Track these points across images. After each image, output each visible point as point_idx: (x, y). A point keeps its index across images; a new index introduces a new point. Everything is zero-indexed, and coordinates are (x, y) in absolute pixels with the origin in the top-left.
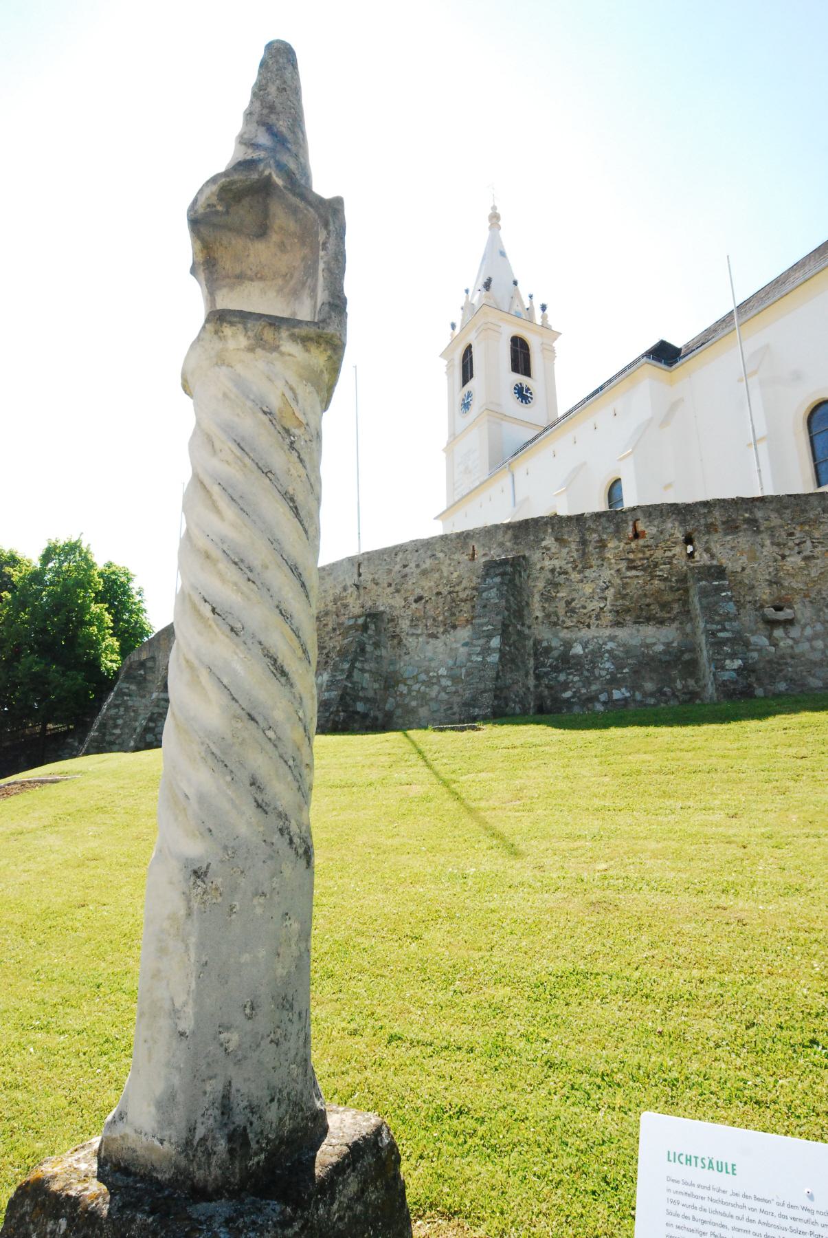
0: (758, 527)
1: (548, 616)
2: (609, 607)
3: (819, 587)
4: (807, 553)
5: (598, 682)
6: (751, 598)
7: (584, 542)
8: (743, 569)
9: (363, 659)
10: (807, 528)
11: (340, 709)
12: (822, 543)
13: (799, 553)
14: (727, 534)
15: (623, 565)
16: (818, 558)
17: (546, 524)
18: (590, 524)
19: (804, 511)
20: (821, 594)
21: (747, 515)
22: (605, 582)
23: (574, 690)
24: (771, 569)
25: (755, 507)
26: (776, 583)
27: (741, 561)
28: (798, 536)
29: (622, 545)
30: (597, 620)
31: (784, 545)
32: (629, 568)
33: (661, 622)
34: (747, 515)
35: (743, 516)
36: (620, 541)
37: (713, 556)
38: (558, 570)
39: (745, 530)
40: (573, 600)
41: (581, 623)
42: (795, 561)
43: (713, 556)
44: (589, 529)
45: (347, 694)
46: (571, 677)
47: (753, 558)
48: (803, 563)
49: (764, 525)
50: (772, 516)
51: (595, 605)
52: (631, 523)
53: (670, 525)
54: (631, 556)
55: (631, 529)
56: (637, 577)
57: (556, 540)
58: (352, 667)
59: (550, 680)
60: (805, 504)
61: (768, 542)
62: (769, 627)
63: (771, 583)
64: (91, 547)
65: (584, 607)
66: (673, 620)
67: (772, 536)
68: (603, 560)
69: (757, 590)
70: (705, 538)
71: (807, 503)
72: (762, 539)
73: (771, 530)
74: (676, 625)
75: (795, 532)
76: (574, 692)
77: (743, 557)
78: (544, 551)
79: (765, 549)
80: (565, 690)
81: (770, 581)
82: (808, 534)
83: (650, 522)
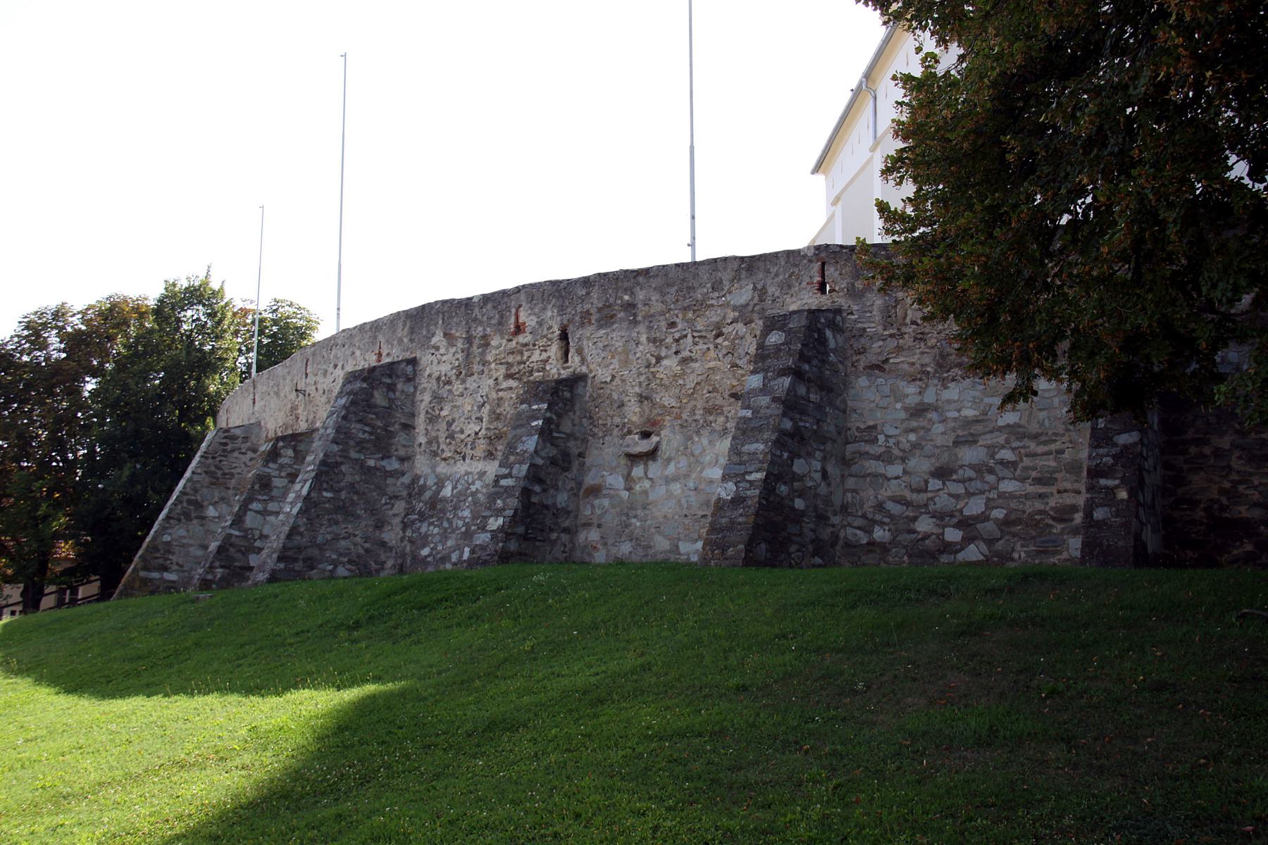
0: (635, 315)
1: (429, 443)
2: (483, 432)
3: (695, 403)
4: (686, 354)
5: (454, 536)
6: (619, 420)
7: (469, 340)
8: (613, 377)
9: (265, 497)
10: (690, 315)
11: (217, 564)
12: (705, 337)
13: (676, 353)
14: (600, 327)
15: (502, 370)
16: (696, 361)
17: (438, 312)
19: (691, 289)
20: (695, 414)
21: (626, 297)
22: (482, 396)
23: (432, 545)
24: (642, 378)
25: (638, 284)
26: (647, 398)
27: (612, 367)
28: (680, 326)
29: (504, 342)
30: (472, 449)
31: (662, 341)
32: (509, 376)
34: (626, 297)
35: (621, 298)
36: (502, 338)
38: (443, 378)
39: (622, 320)
40: (454, 420)
41: (458, 453)
42: (671, 363)
43: (583, 361)
44: (475, 320)
45: (231, 545)
46: (431, 528)
47: (625, 363)
48: (679, 368)
49: (642, 311)
50: (653, 298)
51: (473, 428)
52: (513, 311)
53: (549, 314)
54: (510, 359)
55: (513, 320)
56: (511, 388)
57: (445, 335)
58: (245, 507)
59: (413, 532)
60: (694, 278)
61: (643, 338)
62: (629, 463)
63: (642, 398)
64: (225, 284)
65: (462, 432)
67: (650, 328)
68: (484, 365)
69: (626, 408)
71: (696, 276)
72: (638, 333)
73: (650, 317)
75: (678, 320)
76: (432, 549)
77: (614, 361)
78: (433, 351)
79: (641, 348)
80: (424, 546)
81: (640, 395)
82: (691, 323)
83: (531, 309)
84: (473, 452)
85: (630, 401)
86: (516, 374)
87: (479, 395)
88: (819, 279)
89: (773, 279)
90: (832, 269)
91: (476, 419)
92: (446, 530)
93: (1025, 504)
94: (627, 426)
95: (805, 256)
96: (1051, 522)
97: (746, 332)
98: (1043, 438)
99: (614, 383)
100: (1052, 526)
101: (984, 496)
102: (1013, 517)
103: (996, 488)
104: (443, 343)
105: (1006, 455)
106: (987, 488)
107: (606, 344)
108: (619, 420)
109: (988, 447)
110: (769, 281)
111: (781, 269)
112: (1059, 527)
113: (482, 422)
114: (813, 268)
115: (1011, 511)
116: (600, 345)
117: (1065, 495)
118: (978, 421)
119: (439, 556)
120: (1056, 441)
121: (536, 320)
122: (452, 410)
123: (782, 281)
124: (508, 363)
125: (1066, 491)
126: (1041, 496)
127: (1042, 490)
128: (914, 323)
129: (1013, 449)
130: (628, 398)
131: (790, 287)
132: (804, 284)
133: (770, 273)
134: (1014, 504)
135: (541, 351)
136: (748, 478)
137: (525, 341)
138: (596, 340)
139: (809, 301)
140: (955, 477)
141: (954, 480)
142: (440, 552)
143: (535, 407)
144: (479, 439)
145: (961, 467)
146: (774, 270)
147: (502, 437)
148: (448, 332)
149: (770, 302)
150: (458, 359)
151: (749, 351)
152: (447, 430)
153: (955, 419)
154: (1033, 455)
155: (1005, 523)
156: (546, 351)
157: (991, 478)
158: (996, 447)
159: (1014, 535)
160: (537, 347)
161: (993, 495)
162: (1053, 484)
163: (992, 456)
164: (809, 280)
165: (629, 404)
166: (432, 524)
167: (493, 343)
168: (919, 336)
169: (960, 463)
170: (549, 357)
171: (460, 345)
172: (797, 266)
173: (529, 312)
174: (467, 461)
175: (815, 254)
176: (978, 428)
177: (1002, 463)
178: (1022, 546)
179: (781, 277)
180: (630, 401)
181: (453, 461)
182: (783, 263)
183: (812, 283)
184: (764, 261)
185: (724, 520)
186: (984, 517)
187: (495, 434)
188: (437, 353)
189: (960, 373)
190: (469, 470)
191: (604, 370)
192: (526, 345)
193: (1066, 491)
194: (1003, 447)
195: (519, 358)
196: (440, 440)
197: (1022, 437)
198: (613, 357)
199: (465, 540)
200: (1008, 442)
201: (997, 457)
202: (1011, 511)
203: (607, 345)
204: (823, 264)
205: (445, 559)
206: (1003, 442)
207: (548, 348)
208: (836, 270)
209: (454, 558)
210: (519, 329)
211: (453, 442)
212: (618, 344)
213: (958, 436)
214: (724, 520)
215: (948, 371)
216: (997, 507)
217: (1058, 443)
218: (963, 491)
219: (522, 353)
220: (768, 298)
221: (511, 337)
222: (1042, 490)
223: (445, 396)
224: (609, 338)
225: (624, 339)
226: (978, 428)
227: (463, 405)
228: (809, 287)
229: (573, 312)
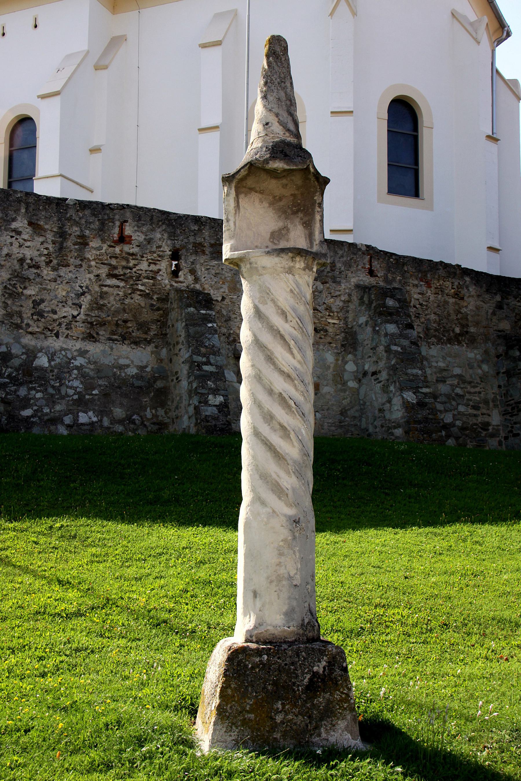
2: (82, 317)
5: (64, 402)
7: (62, 235)
8: (223, 299)
18: (71, 212)
23: (35, 408)
27: (222, 290)
29: (105, 247)
33: (136, 343)
37: (197, 280)
40: (42, 301)
43: (197, 280)
51: (69, 311)
52: (118, 223)
54: (114, 262)
55: (117, 230)
56: (118, 287)
57: (30, 224)
65: (54, 312)
66: (149, 342)
69: (232, 323)
70: (192, 258)
74: (150, 348)
78: (13, 234)
80: (24, 408)
83: (138, 227)
84: (68, 332)
85: (236, 318)
86: (121, 275)
87: (77, 285)
88: (369, 266)
89: (340, 258)
90: (376, 263)
91: (73, 304)
92: (52, 395)
93: (469, 419)
94: (232, 336)
95: (360, 249)
96: (480, 430)
97: (323, 289)
98: (473, 384)
99: (225, 302)
100: (481, 432)
101: (452, 413)
102: (465, 426)
103: (457, 409)
104: (27, 230)
105: (458, 391)
106: (452, 408)
107: (217, 272)
108: (226, 330)
109: (451, 385)
110: (337, 259)
111: (345, 253)
112: (484, 433)
113: (80, 307)
114: (365, 258)
115: (464, 423)
116: (213, 272)
117: (485, 416)
118: (445, 370)
119: (46, 418)
120: (477, 386)
121: (143, 237)
122: (40, 291)
123: (345, 261)
124: (110, 265)
125: (484, 414)
126: (475, 416)
127: (475, 412)
128: (415, 306)
129: (462, 388)
130: (235, 316)
131: (350, 266)
132: (360, 267)
133: (338, 254)
134: (464, 419)
135: (150, 263)
136: (420, 390)
137: (131, 251)
138: (208, 267)
139: (364, 279)
140: (438, 400)
141: (438, 402)
142: (47, 414)
143: (203, 312)
144: (76, 322)
145: (441, 395)
146: (340, 252)
147: (105, 324)
148: (33, 221)
149: (338, 273)
150: (47, 249)
151: (326, 302)
152: (33, 308)
153: (436, 367)
154: (470, 393)
155: (463, 429)
156: (155, 264)
157: (454, 403)
158: (454, 386)
159: (467, 436)
160: (145, 259)
161: (455, 413)
162: (479, 410)
163: (453, 390)
164: (363, 265)
165: (235, 320)
166: (34, 388)
167: (92, 244)
168: (417, 315)
169: (439, 392)
170: (160, 270)
171: (50, 236)
172: (355, 254)
173: (136, 228)
174: (61, 339)
175: (367, 250)
176: (445, 374)
177: (457, 395)
178: (471, 442)
179: (345, 259)
180: (236, 318)
181: (43, 336)
182: (346, 250)
183: (365, 268)
184: (334, 244)
185: (419, 416)
186: (452, 425)
187: (97, 321)
188: (18, 237)
189: (435, 341)
190: (65, 346)
191: (216, 291)
192: (133, 254)
193: (484, 414)
194: (457, 387)
195: (124, 263)
196: (25, 316)
197: (464, 382)
198: (223, 283)
199: (78, 406)
200: (458, 384)
201: (455, 391)
202: (464, 423)
203: (218, 273)
204: (371, 258)
205: (55, 420)
206: (456, 384)
207: (158, 262)
208: (378, 264)
209: (68, 420)
210: (123, 239)
211: (43, 320)
212: (227, 275)
213: (437, 377)
214: (419, 416)
215: (430, 339)
216: (458, 420)
217: (479, 388)
218: (443, 409)
219: (128, 262)
220: (337, 270)
221: (113, 244)
222: (475, 412)
223: (31, 278)
224: (220, 268)
225: (232, 272)
226: (445, 374)
227: (55, 290)
228: (363, 270)
229: (186, 240)
